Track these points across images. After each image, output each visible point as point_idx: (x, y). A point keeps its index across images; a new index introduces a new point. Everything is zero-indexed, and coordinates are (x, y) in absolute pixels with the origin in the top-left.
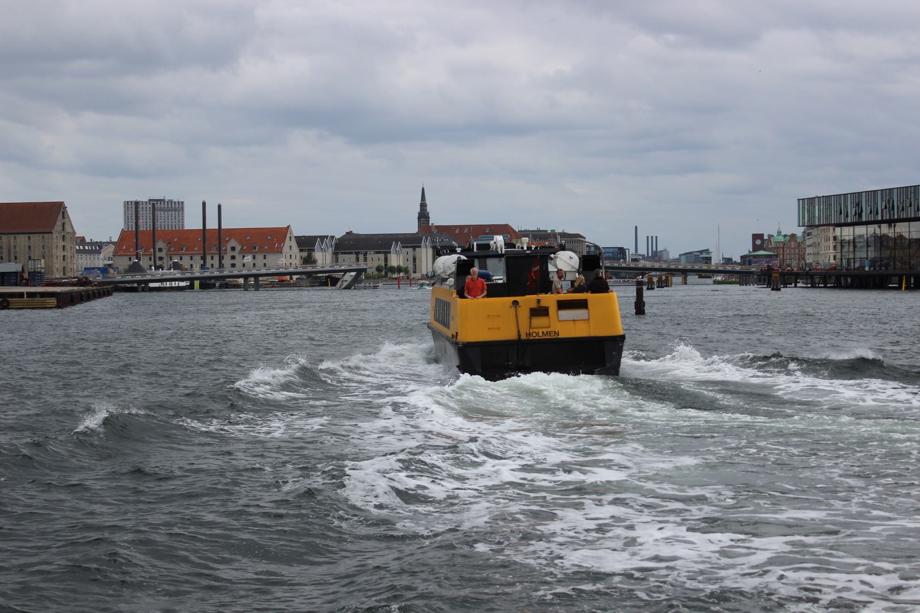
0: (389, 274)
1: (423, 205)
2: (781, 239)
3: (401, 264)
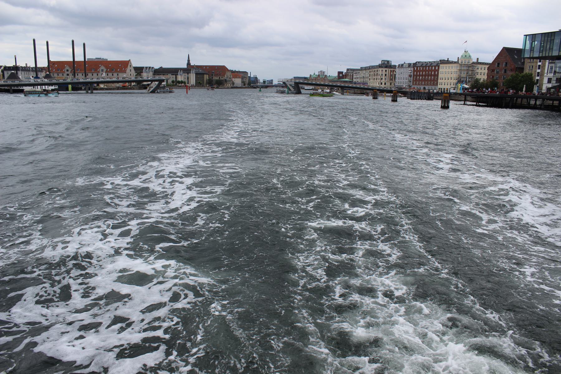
0: (177, 84)
1: (189, 61)
2: (315, 76)
3: (183, 80)
